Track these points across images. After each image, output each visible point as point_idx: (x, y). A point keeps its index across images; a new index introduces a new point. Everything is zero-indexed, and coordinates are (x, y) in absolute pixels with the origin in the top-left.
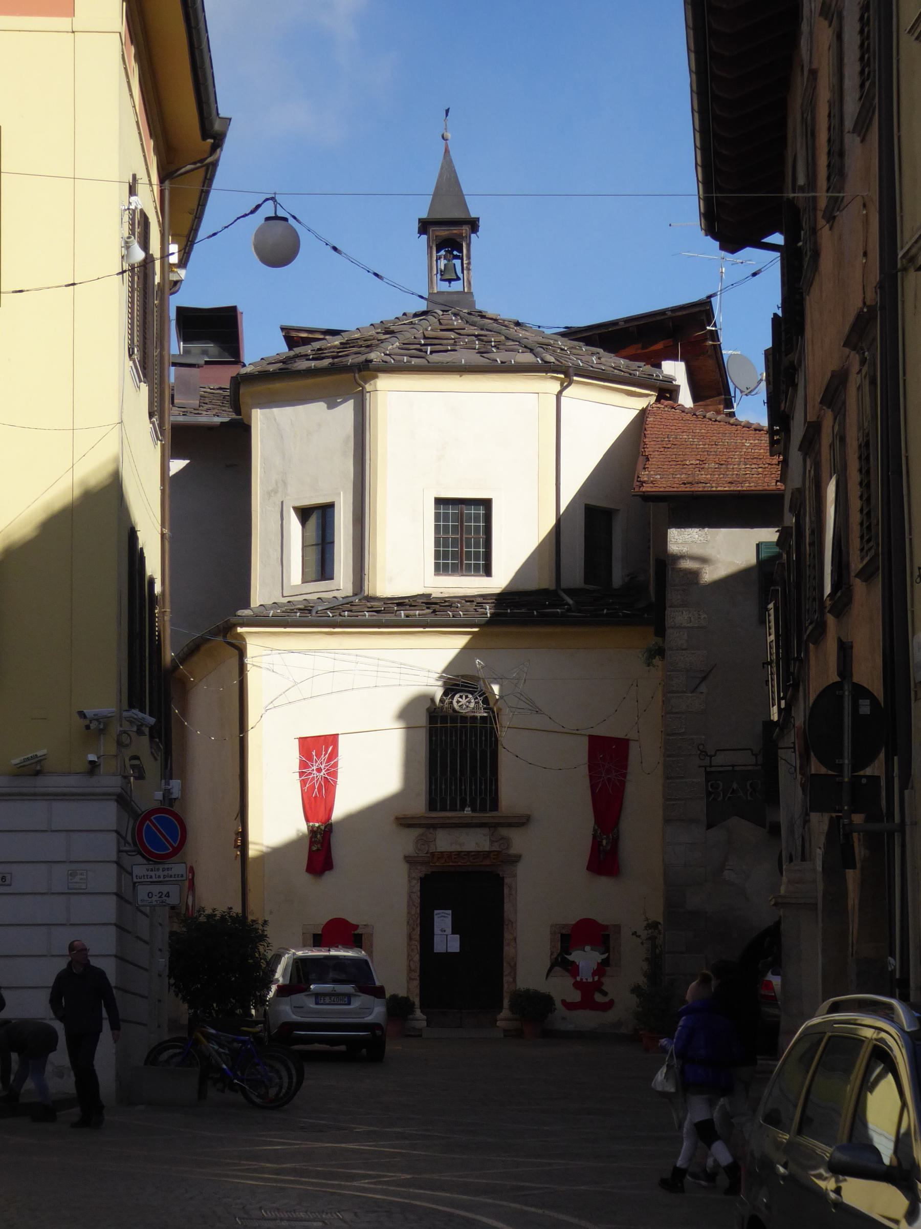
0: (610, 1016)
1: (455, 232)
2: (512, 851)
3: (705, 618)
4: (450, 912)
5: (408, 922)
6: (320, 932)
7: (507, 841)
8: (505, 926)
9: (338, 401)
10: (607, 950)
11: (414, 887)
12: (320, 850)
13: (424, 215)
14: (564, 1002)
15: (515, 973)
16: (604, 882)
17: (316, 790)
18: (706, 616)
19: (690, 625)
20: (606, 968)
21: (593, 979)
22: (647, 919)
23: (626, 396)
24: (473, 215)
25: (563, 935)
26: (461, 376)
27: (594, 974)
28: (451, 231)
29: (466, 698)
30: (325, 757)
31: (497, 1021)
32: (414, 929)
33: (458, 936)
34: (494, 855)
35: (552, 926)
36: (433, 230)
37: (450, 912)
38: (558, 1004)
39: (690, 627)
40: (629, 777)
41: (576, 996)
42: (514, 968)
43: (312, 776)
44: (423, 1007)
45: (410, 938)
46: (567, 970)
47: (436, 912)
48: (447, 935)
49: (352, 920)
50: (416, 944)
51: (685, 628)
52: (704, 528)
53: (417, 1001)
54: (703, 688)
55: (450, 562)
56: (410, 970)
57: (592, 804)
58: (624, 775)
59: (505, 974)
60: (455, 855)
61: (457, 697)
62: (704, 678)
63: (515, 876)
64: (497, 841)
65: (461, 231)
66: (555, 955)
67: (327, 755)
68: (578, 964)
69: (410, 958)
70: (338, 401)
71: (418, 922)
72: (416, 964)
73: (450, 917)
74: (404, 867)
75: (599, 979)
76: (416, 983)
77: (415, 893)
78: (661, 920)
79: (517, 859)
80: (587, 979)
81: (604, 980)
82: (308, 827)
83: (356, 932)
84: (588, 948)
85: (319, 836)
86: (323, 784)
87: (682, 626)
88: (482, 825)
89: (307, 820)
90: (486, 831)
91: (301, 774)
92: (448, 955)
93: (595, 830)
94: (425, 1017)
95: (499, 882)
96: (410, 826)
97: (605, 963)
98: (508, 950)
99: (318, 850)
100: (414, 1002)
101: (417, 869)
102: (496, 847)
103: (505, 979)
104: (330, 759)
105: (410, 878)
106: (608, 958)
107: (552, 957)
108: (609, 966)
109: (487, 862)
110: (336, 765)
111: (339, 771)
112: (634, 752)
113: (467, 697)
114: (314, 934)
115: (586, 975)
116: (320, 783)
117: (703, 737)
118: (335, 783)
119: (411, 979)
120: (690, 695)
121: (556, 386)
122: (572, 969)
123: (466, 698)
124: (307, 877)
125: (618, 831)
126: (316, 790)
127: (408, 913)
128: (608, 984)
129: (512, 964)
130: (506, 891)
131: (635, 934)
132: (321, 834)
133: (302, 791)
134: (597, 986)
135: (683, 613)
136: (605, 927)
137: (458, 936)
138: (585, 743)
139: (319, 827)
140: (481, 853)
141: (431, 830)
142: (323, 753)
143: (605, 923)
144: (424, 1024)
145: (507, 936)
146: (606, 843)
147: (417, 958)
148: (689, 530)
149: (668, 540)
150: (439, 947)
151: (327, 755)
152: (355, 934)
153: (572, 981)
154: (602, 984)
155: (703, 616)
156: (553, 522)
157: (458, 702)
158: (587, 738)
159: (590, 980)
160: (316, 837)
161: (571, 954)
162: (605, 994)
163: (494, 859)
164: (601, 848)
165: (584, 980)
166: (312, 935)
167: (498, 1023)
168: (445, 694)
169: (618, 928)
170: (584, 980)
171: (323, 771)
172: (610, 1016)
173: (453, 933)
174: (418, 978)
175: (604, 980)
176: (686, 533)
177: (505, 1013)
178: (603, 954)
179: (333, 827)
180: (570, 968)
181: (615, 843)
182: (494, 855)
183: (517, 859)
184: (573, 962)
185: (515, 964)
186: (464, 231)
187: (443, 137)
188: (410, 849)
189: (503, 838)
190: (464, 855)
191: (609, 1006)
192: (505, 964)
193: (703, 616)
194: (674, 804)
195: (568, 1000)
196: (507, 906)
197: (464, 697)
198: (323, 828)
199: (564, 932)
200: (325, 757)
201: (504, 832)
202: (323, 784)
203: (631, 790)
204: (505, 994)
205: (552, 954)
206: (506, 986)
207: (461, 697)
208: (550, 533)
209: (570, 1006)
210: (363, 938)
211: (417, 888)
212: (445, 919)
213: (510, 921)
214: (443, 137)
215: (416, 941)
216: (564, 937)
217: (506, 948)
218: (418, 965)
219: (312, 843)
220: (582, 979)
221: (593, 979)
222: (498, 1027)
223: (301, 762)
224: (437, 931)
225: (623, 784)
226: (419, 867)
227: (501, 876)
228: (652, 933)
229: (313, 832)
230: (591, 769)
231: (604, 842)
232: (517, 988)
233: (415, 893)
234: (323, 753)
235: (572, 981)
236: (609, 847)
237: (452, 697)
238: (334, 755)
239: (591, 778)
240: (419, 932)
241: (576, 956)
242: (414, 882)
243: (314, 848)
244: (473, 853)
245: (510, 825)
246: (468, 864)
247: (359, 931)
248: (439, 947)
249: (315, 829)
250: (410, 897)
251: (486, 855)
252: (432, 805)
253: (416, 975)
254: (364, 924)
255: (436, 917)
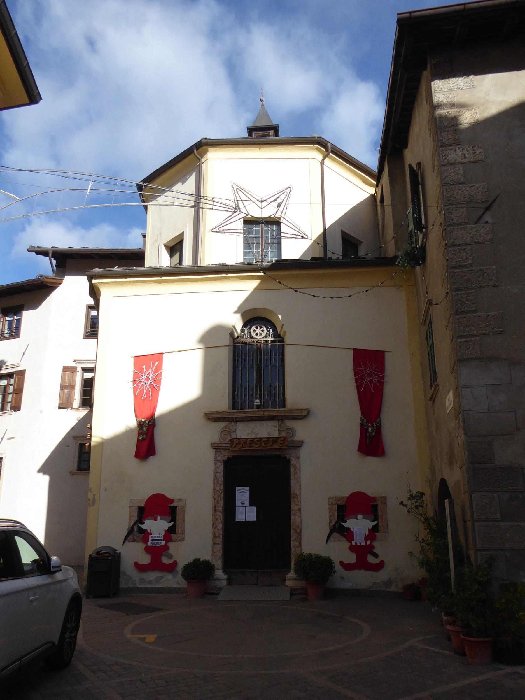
0: (382, 576)
1: (266, 133)
2: (297, 438)
3: (480, 152)
4: (248, 488)
5: (214, 497)
6: (143, 505)
7: (291, 431)
8: (292, 499)
9: (188, 177)
10: (376, 518)
11: (218, 468)
12: (145, 439)
13: (250, 125)
14: (341, 563)
15: (300, 538)
16: (372, 461)
17: (145, 394)
18: (481, 150)
19: (466, 160)
20: (376, 533)
21: (366, 543)
22: (410, 491)
23: (363, 183)
24: (275, 123)
25: (339, 506)
26: (259, 149)
27: (366, 539)
28: (264, 134)
29: (260, 328)
30: (152, 369)
31: (285, 580)
32: (218, 502)
33: (254, 508)
34: (281, 441)
35: (330, 498)
36: (254, 134)
37: (248, 488)
38: (337, 566)
39: (465, 163)
40: (386, 379)
41: (352, 558)
42: (299, 534)
43: (142, 384)
44: (226, 568)
45: (215, 510)
46: (344, 536)
47: (237, 488)
48: (246, 507)
49: (169, 495)
50: (220, 515)
51: (461, 163)
52: (468, 75)
53: (218, 563)
54: (488, 217)
55: (249, 250)
56: (215, 536)
57: (359, 404)
58: (383, 378)
59: (292, 539)
60: (250, 441)
61: (253, 328)
62: (487, 209)
63: (299, 458)
64: (284, 431)
65: (269, 133)
66: (333, 523)
67: (154, 368)
68: (352, 530)
69: (214, 527)
70: (188, 177)
71: (222, 496)
72: (220, 532)
73: (248, 492)
74: (211, 453)
75: (371, 542)
76: (219, 547)
77: (219, 473)
78: (428, 492)
79: (301, 444)
80: (360, 543)
81: (375, 544)
82: (137, 421)
83: (172, 505)
84: (360, 516)
85: (144, 429)
86: (150, 390)
87: (457, 162)
88: (272, 418)
89: (137, 417)
90: (275, 423)
91: (134, 382)
92: (247, 524)
93: (362, 420)
94: (225, 577)
95: (286, 464)
96: (216, 420)
97: (375, 529)
98: (294, 519)
99: (143, 439)
100: (214, 565)
101: (221, 454)
102: (283, 435)
103: (293, 543)
104: (155, 372)
105: (216, 461)
106: (377, 525)
107: (331, 525)
108: (378, 532)
109: (276, 446)
110: (160, 374)
111: (162, 380)
112: (389, 360)
113: (261, 328)
114: (139, 507)
115: (359, 540)
116: (148, 390)
117: (495, 267)
118: (159, 388)
119: (214, 544)
120: (475, 226)
121: (320, 157)
122: (348, 534)
123: (260, 328)
124: (136, 461)
125: (380, 420)
126: (145, 394)
127: (214, 489)
128: (378, 547)
129: (298, 531)
130: (292, 470)
131: (401, 503)
132: (146, 427)
133: (135, 395)
134: (369, 550)
135: (455, 151)
136: (374, 499)
137: (254, 508)
138: (350, 355)
139: (145, 422)
140: (271, 439)
141: (233, 423)
142: (151, 367)
143: (374, 496)
144: (225, 583)
145: (293, 507)
146: (371, 430)
147: (220, 526)
148: (454, 80)
149: (433, 90)
150: (240, 517)
151: (154, 368)
152: (170, 507)
153: (348, 545)
154: (373, 547)
155: (477, 152)
156: (321, 231)
157: (254, 331)
158: (351, 352)
159: (363, 544)
160: (142, 429)
161: (346, 522)
162: (376, 556)
163: (281, 443)
164: (368, 434)
165: (358, 544)
166: (137, 508)
167: (287, 583)
168: (245, 325)
169: (384, 499)
170: (358, 544)
171: (150, 380)
172: (382, 576)
173: (251, 505)
174: (221, 543)
175: (375, 544)
176: (450, 82)
177: (292, 574)
178: (373, 521)
179: (157, 422)
180: (346, 533)
181: (378, 430)
182: (281, 441)
183: (301, 444)
184: (348, 529)
185: (301, 531)
186: (271, 133)
187: (261, 100)
188: (216, 438)
189: (289, 429)
190: (258, 441)
191: (379, 567)
192: (292, 531)
193: (477, 152)
194: (467, 341)
195: (346, 562)
196: (293, 483)
197: (259, 328)
198: (147, 422)
199: (340, 503)
200: (152, 369)
201: (289, 423)
202: (150, 390)
203: (389, 390)
204: (292, 557)
205: (330, 522)
206: (293, 549)
207: (257, 328)
208: (319, 236)
209: (347, 567)
210: (177, 509)
211: (221, 468)
212: (244, 493)
213: (296, 494)
214: (261, 100)
215: (220, 512)
216: (340, 508)
217: (292, 517)
218: (221, 532)
219: (139, 434)
220: (356, 543)
221: (366, 543)
222: (287, 586)
223: (135, 373)
224: (238, 504)
225: (382, 384)
226: (223, 453)
227: (288, 458)
228: (416, 502)
229: (140, 425)
230: (356, 373)
231: (370, 429)
232: (302, 552)
233: (219, 473)
234: (151, 367)
235: (348, 545)
236: (374, 434)
237: (250, 328)
238: (159, 368)
239: (357, 380)
240: (222, 505)
241: (350, 523)
242: (219, 464)
243: (140, 438)
244: (264, 440)
245: (294, 418)
246: (261, 448)
247: (174, 504)
248: (240, 517)
249: (142, 423)
250: (215, 476)
251: (275, 440)
252: (234, 405)
253: (220, 540)
254: (179, 498)
255: (237, 492)
